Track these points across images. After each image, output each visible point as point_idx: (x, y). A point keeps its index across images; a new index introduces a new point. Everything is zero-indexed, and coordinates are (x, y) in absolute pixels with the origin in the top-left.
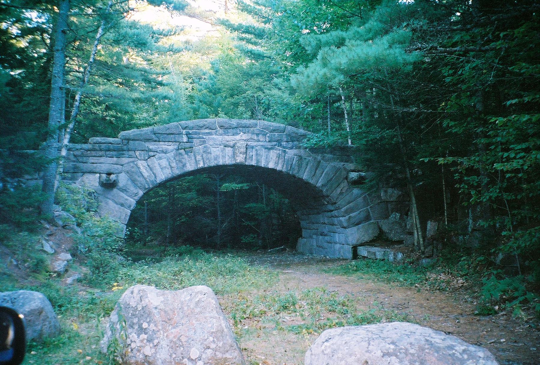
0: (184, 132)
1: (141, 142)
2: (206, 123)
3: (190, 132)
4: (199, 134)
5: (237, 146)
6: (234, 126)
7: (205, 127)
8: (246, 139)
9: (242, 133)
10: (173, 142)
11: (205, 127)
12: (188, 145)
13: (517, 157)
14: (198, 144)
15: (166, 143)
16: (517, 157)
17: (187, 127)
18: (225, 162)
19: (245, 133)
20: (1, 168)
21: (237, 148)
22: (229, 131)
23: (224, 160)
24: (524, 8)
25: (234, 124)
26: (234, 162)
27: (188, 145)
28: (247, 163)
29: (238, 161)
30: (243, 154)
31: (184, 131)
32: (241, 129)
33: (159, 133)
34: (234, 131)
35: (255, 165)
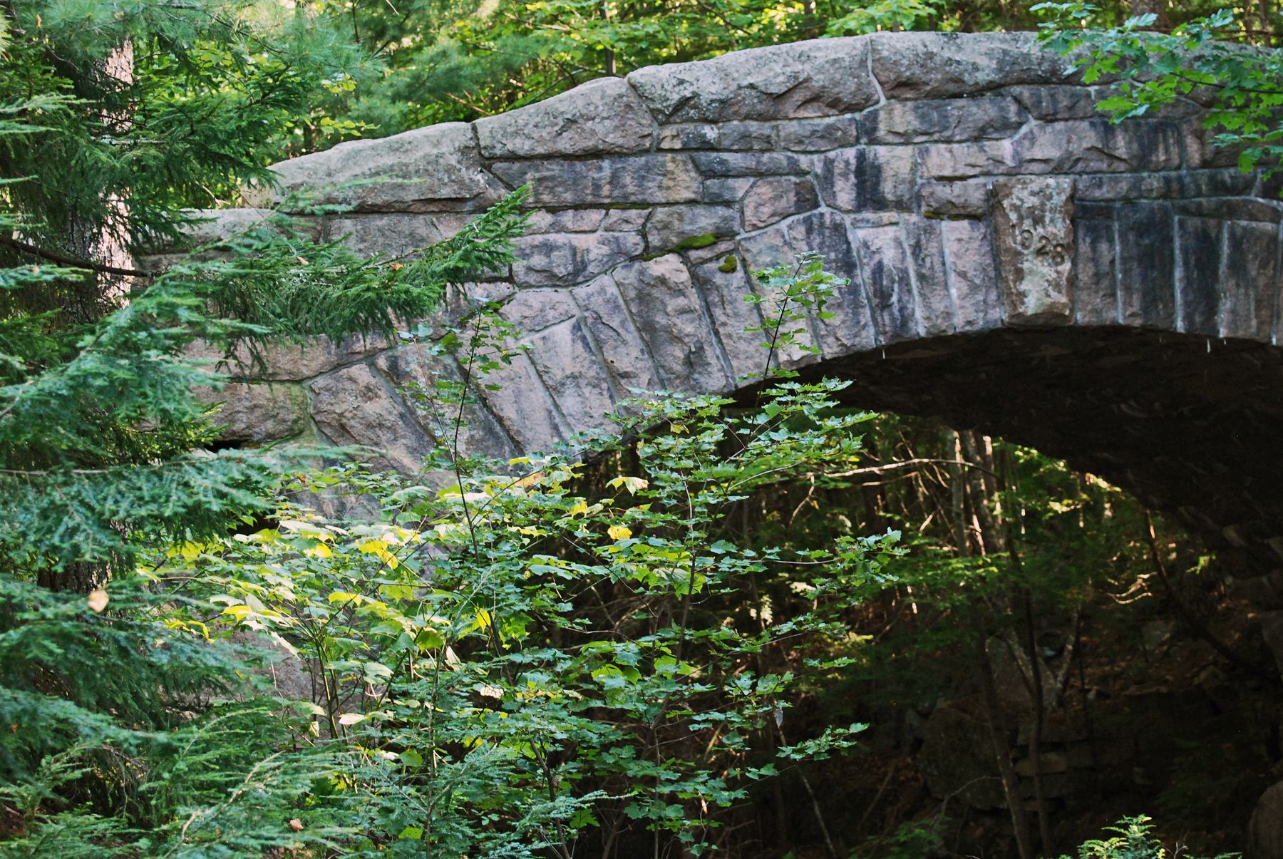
0: (670, 136)
1: (405, 223)
2: (805, 69)
3: (710, 132)
4: (769, 145)
5: (1016, 208)
6: (982, 77)
7: (799, 97)
8: (1061, 162)
9: (1033, 123)
10: (607, 207)
11: (799, 97)
12: (705, 220)
13: (148, 126)
14: (767, 210)
15: (568, 218)
16: (148, 126)
17: (684, 102)
18: (948, 315)
19: (1049, 119)
20: (694, 1)
21: (1013, 217)
22: (955, 108)
23: (939, 306)
24: (168, 211)
25: (983, 61)
26: (999, 315)
27: (705, 220)
28: (1081, 318)
29: (1031, 305)
30: (1057, 259)
31: (669, 131)
32: (1025, 92)
33: (513, 157)
34: (983, 111)
35: (1138, 322)
